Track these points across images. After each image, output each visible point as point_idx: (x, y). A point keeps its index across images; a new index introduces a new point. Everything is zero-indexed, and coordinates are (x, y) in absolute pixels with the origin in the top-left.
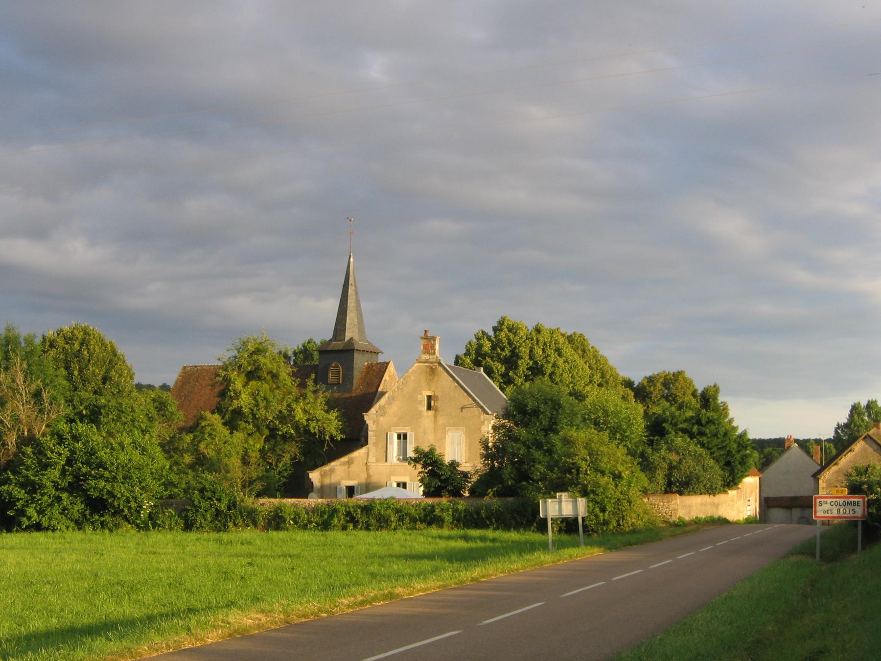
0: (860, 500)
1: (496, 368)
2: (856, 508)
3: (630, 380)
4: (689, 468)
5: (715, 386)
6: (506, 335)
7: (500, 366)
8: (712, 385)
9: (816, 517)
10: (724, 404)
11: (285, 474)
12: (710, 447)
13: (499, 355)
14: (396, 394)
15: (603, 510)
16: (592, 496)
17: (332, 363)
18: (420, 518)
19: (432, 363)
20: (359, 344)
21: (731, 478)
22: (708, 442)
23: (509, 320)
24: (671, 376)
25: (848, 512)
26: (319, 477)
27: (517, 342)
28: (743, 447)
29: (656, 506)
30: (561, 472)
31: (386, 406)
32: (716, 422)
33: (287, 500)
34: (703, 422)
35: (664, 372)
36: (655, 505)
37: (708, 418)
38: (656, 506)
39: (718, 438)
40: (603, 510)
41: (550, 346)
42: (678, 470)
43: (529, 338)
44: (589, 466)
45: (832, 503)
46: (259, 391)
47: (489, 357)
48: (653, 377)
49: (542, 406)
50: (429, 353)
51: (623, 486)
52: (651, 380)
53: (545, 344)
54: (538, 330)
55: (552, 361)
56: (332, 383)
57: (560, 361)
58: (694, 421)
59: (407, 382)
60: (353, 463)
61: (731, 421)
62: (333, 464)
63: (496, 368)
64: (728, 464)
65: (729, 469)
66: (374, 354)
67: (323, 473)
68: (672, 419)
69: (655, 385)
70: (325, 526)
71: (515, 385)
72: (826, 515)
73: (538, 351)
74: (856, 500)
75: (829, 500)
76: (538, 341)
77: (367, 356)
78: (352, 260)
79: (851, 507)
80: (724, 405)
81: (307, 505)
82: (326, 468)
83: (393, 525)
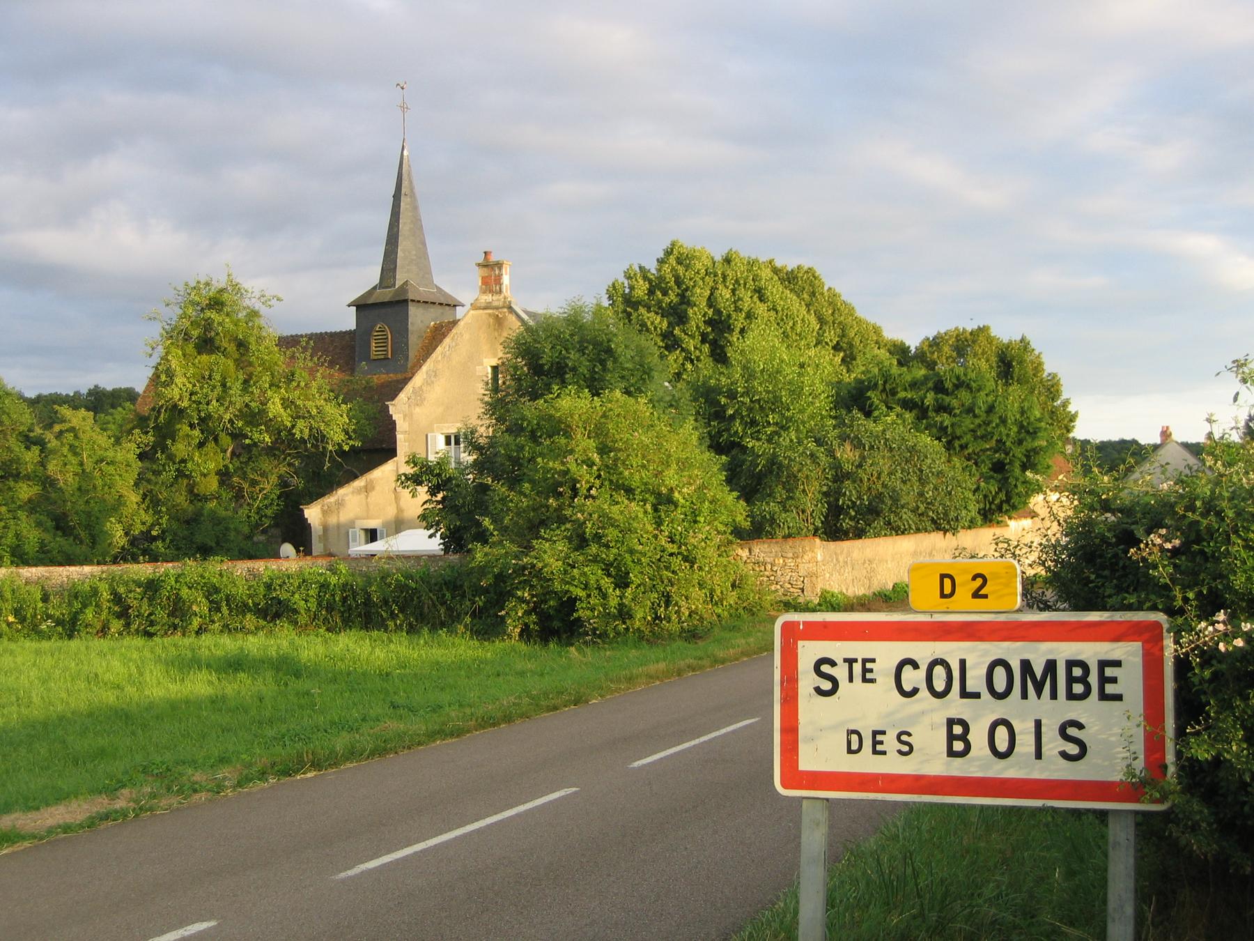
0: (1129, 652)
1: (652, 323)
2: (1089, 711)
3: (903, 343)
4: (879, 478)
5: (1022, 340)
6: (673, 269)
7: (658, 320)
8: (1019, 338)
9: (794, 777)
10: (1053, 376)
11: (269, 512)
12: (958, 434)
13: (660, 302)
14: (440, 367)
15: (622, 582)
16: (594, 549)
17: (376, 325)
18: (256, 605)
19: (497, 308)
20: (419, 290)
21: (1002, 496)
22: (953, 425)
23: (681, 246)
24: (968, 334)
25: (1025, 743)
26: (321, 516)
27: (691, 279)
28: (1028, 432)
29: (769, 567)
30: (538, 493)
31: (424, 388)
32: (974, 385)
33: (30, 569)
34: (948, 385)
35: (957, 329)
36: (765, 564)
37: (958, 378)
38: (769, 567)
39: (975, 416)
40: (622, 582)
41: (745, 284)
42: (854, 482)
43: (711, 273)
44: (599, 477)
45: (912, 678)
46: (212, 370)
47: (644, 307)
48: (938, 338)
49: (573, 355)
50: (491, 291)
51: (675, 521)
52: (935, 343)
53: (737, 281)
54: (728, 261)
55: (746, 308)
56: (376, 357)
57: (761, 309)
58: (930, 384)
59: (456, 345)
60: (373, 488)
61: (1065, 404)
62: (341, 492)
63: (652, 323)
64: (999, 467)
65: (1000, 476)
66: (447, 308)
67: (326, 508)
68: (885, 382)
69: (940, 350)
70: (70, 627)
71: (683, 350)
72: (865, 763)
73: (725, 293)
74: (1091, 651)
75: (887, 654)
76: (724, 277)
77: (439, 310)
78: (405, 153)
79: (1054, 711)
80: (1054, 378)
81: (65, 579)
82: (330, 500)
83: (196, 622)
